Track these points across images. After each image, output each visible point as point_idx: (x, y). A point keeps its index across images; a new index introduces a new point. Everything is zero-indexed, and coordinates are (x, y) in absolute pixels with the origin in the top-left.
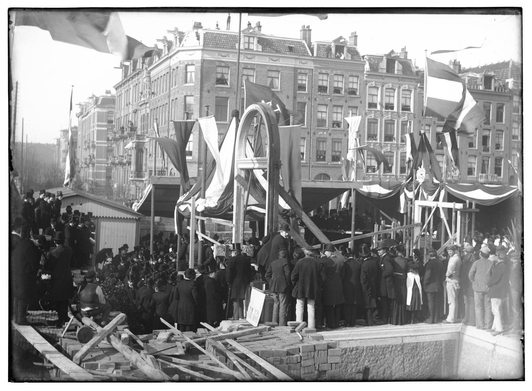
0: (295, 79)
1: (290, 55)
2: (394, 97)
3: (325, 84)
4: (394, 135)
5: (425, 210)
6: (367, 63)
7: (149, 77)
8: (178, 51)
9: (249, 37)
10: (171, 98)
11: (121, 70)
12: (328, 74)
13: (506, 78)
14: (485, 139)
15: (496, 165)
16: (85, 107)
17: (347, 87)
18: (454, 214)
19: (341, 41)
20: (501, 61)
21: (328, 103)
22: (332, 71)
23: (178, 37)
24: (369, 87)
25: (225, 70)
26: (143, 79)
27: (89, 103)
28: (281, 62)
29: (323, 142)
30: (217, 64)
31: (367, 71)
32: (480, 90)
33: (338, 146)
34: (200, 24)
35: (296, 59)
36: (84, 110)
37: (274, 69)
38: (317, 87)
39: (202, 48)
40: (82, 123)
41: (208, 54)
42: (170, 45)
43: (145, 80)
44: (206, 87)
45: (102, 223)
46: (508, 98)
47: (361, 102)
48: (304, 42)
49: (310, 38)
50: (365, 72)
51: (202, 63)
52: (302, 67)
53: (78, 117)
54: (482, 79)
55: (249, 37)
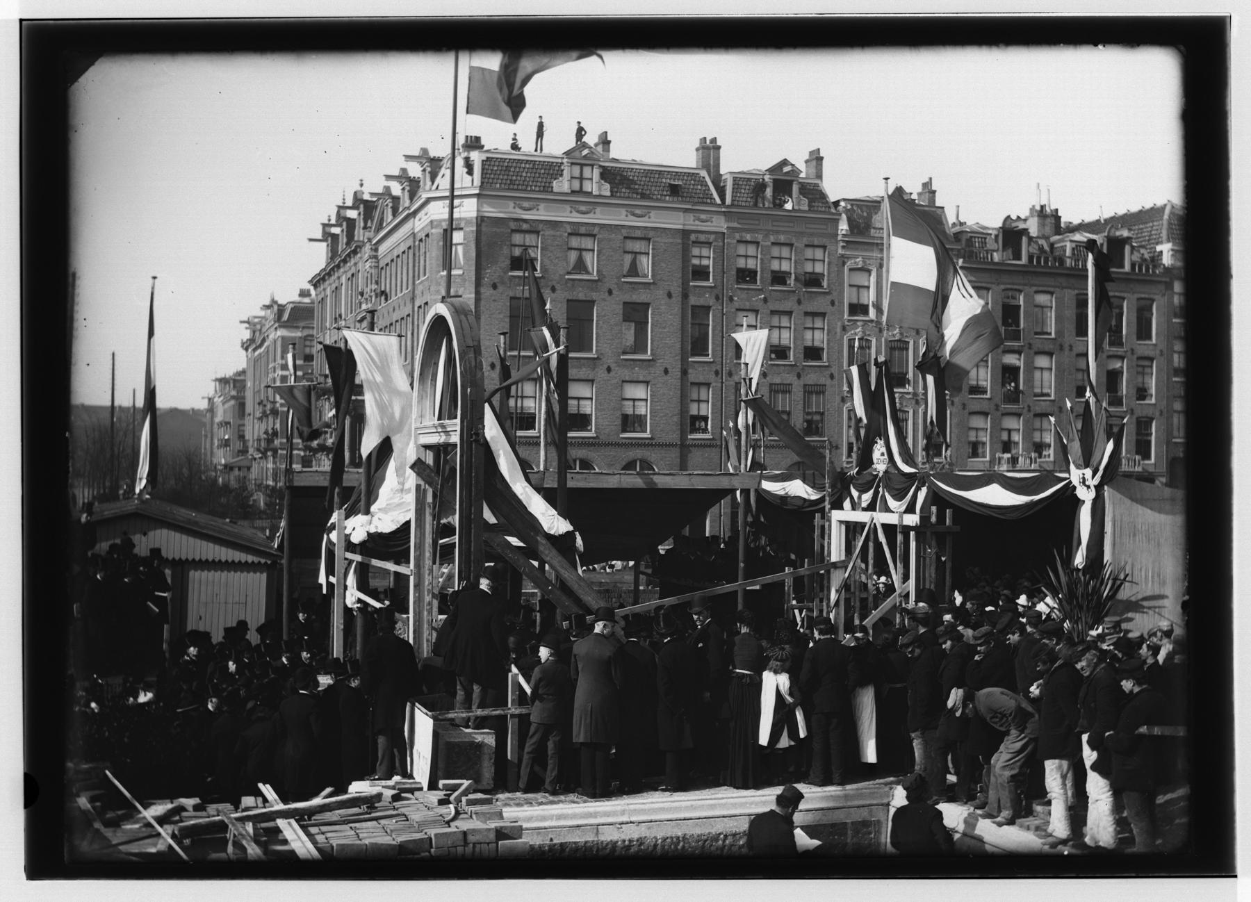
0: (686, 255)
1: (673, 202)
2: (868, 287)
3: (751, 264)
4: (907, 372)
5: (852, 529)
6: (844, 216)
7: (376, 257)
8: (428, 201)
9: (582, 165)
10: (417, 304)
11: (325, 244)
12: (758, 243)
13: (1157, 244)
14: (1112, 379)
15: (1138, 434)
16: (258, 327)
17: (800, 271)
18: (900, 538)
19: (787, 169)
20: (1148, 206)
21: (760, 306)
22: (766, 236)
23: (429, 169)
24: (851, 270)
25: (530, 239)
26: (363, 262)
27: (264, 318)
28: (653, 219)
29: (818, 393)
30: (513, 225)
31: (844, 235)
32: (992, 263)
33: (784, 400)
34: (478, 139)
35: (686, 210)
36: (257, 334)
37: (638, 234)
38: (734, 272)
39: (477, 192)
40: (255, 362)
41: (490, 205)
42: (413, 186)
43: (368, 264)
44: (490, 274)
45: (192, 573)
46: (1162, 287)
47: (833, 303)
48: (704, 173)
49: (717, 166)
50: (840, 238)
51: (478, 226)
52: (700, 228)
53: (246, 349)
54: (997, 236)
55: (582, 165)
